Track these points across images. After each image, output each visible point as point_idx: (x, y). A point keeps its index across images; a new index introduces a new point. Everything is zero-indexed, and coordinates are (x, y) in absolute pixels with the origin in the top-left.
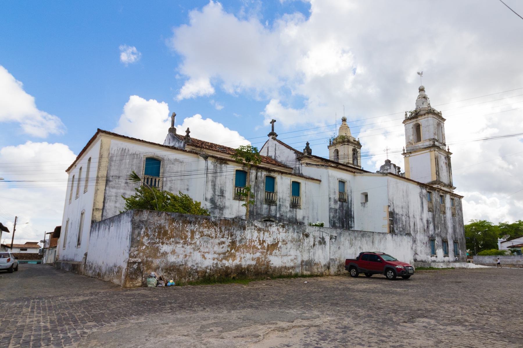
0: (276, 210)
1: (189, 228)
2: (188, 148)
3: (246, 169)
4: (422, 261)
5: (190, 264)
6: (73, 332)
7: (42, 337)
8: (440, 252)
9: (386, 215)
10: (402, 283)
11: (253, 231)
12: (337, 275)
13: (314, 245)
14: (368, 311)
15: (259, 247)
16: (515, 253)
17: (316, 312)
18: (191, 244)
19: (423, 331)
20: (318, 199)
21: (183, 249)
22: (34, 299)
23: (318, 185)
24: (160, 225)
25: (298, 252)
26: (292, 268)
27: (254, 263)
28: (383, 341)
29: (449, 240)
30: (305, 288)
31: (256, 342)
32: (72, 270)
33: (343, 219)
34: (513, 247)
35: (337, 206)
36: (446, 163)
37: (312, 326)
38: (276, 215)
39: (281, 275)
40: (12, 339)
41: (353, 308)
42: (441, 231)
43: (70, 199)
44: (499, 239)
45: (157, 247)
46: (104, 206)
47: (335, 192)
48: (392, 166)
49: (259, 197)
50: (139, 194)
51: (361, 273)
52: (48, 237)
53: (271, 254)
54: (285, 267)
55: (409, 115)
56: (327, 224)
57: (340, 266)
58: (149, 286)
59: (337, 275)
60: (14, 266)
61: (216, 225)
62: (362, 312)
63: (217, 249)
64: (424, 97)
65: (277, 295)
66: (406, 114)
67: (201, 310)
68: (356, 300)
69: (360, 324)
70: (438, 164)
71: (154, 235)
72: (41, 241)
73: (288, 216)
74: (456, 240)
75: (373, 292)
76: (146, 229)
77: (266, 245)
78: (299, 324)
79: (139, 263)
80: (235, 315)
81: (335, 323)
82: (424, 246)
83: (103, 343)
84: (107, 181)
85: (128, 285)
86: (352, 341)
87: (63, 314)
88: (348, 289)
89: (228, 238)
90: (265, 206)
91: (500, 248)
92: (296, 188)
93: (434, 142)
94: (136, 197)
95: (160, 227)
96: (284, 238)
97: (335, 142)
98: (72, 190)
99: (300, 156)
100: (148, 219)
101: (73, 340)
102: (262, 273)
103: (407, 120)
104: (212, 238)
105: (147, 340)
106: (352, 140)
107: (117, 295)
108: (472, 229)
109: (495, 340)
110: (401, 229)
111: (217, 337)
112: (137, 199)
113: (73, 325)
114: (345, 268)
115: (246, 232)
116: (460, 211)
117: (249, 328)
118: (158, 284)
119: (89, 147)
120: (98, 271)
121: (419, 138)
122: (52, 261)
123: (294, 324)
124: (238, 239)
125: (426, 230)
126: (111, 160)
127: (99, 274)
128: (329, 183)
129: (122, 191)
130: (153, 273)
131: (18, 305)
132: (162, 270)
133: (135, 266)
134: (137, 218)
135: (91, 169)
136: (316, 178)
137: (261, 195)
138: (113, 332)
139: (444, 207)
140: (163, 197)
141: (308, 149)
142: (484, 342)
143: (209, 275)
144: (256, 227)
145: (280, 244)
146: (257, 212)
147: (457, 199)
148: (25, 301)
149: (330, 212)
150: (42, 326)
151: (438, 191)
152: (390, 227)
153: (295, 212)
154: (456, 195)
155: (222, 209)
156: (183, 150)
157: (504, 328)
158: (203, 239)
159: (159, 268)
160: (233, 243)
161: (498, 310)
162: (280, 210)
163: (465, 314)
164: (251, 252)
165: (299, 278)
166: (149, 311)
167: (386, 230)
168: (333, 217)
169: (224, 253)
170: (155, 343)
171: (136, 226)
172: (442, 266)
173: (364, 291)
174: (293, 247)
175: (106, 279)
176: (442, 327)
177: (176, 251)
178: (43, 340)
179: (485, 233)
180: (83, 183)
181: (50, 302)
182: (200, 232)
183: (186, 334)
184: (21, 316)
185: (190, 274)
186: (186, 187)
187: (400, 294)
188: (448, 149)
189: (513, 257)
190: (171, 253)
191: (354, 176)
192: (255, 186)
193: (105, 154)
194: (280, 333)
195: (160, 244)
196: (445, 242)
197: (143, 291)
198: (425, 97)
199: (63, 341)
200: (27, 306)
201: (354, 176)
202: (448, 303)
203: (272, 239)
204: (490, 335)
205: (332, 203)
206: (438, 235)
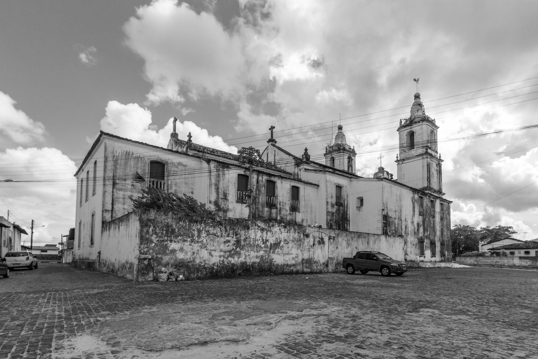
0: (277, 213)
1: (195, 227)
2: (191, 153)
3: (248, 173)
4: (411, 261)
5: (197, 261)
6: (87, 320)
7: (56, 324)
8: (428, 253)
9: (380, 218)
10: (398, 279)
11: (257, 230)
12: (335, 272)
13: (314, 245)
14: (372, 302)
15: (263, 246)
16: (495, 255)
17: (322, 303)
18: (198, 242)
19: (430, 320)
20: (315, 205)
21: (191, 247)
22: (50, 291)
23: (316, 189)
24: (168, 223)
25: (299, 251)
26: (294, 265)
27: (258, 260)
28: (394, 329)
30: (307, 283)
31: (269, 330)
32: (88, 267)
33: (339, 221)
34: (493, 249)
35: (334, 210)
36: (437, 170)
37: (321, 315)
38: (277, 217)
39: (283, 271)
40: (26, 326)
41: (357, 300)
43: (81, 202)
44: (480, 242)
45: (166, 245)
46: (113, 208)
47: (332, 196)
48: (385, 173)
49: (261, 201)
50: (146, 195)
51: (357, 270)
52: (65, 240)
53: (274, 252)
54: (287, 265)
56: (324, 226)
57: (337, 264)
58: (161, 280)
59: (335, 272)
60: (34, 264)
61: (221, 224)
62: (367, 303)
63: (222, 247)
65: (282, 288)
66: (401, 122)
67: (212, 301)
68: (358, 293)
69: (368, 314)
71: (162, 234)
72: (59, 244)
73: (288, 219)
75: (373, 286)
76: (154, 227)
77: (268, 244)
78: (308, 313)
79: (150, 259)
80: (244, 305)
81: (343, 312)
82: (414, 247)
83: (116, 329)
84: (114, 184)
85: (140, 280)
86: (363, 329)
87: (78, 304)
88: (349, 284)
89: (233, 237)
90: (266, 209)
91: (480, 251)
92: (295, 192)
93: (427, 150)
94: (142, 198)
95: (168, 226)
96: (286, 238)
97: (331, 149)
98: (81, 193)
99: (298, 162)
100: (156, 218)
101: (86, 327)
102: (265, 270)
103: (402, 127)
104: (218, 236)
105: (160, 327)
106: (347, 148)
107: (130, 288)
108: (455, 233)
109: (504, 328)
110: (394, 232)
111: (229, 324)
112: (144, 200)
113: (87, 314)
114: (342, 266)
115: (250, 232)
117: (260, 317)
118: (168, 279)
119: (94, 151)
120: (111, 268)
121: (412, 145)
122: (71, 261)
123: (303, 313)
124: (242, 238)
125: (416, 233)
126: (116, 162)
127: (113, 271)
128: (327, 187)
129: (129, 193)
130: (163, 269)
131: (35, 296)
132: (172, 266)
133: (146, 262)
134: (145, 217)
135: (98, 169)
136: (314, 183)
137: (263, 199)
138: (126, 320)
139: (434, 211)
140: (168, 198)
141: (306, 155)
142: (494, 329)
143: (217, 272)
144: (259, 227)
145: (282, 243)
146: (259, 215)
147: (446, 205)
148: (42, 293)
149: (327, 216)
150: (57, 314)
152: (383, 230)
153: (294, 215)
154: (445, 200)
155: (226, 211)
156: (186, 154)
157: (508, 317)
158: (209, 237)
159: (168, 264)
160: (238, 242)
161: (496, 301)
162: (280, 213)
163: (465, 305)
164: (255, 250)
165: (300, 275)
166: (161, 301)
167: (380, 232)
168: (330, 220)
169: (230, 251)
170: (168, 330)
171: (144, 224)
172: (429, 265)
173: (364, 285)
174: (294, 246)
175: (120, 274)
176: (448, 317)
177: (184, 248)
178: (57, 327)
179: (467, 238)
180: (91, 183)
181: (66, 294)
182: (206, 231)
183: (198, 322)
184: (37, 306)
185: (198, 270)
186: (191, 190)
187: (399, 288)
188: (440, 157)
189: (492, 258)
190: (180, 250)
191: (351, 181)
192: (256, 190)
193: (110, 155)
194: (291, 321)
195: (169, 242)
197: (155, 285)
198: (420, 105)
199: (76, 328)
200: (44, 298)
201: (351, 181)
202: (446, 296)
203: (274, 238)
204: (496, 323)
205: (329, 207)
206: (427, 237)
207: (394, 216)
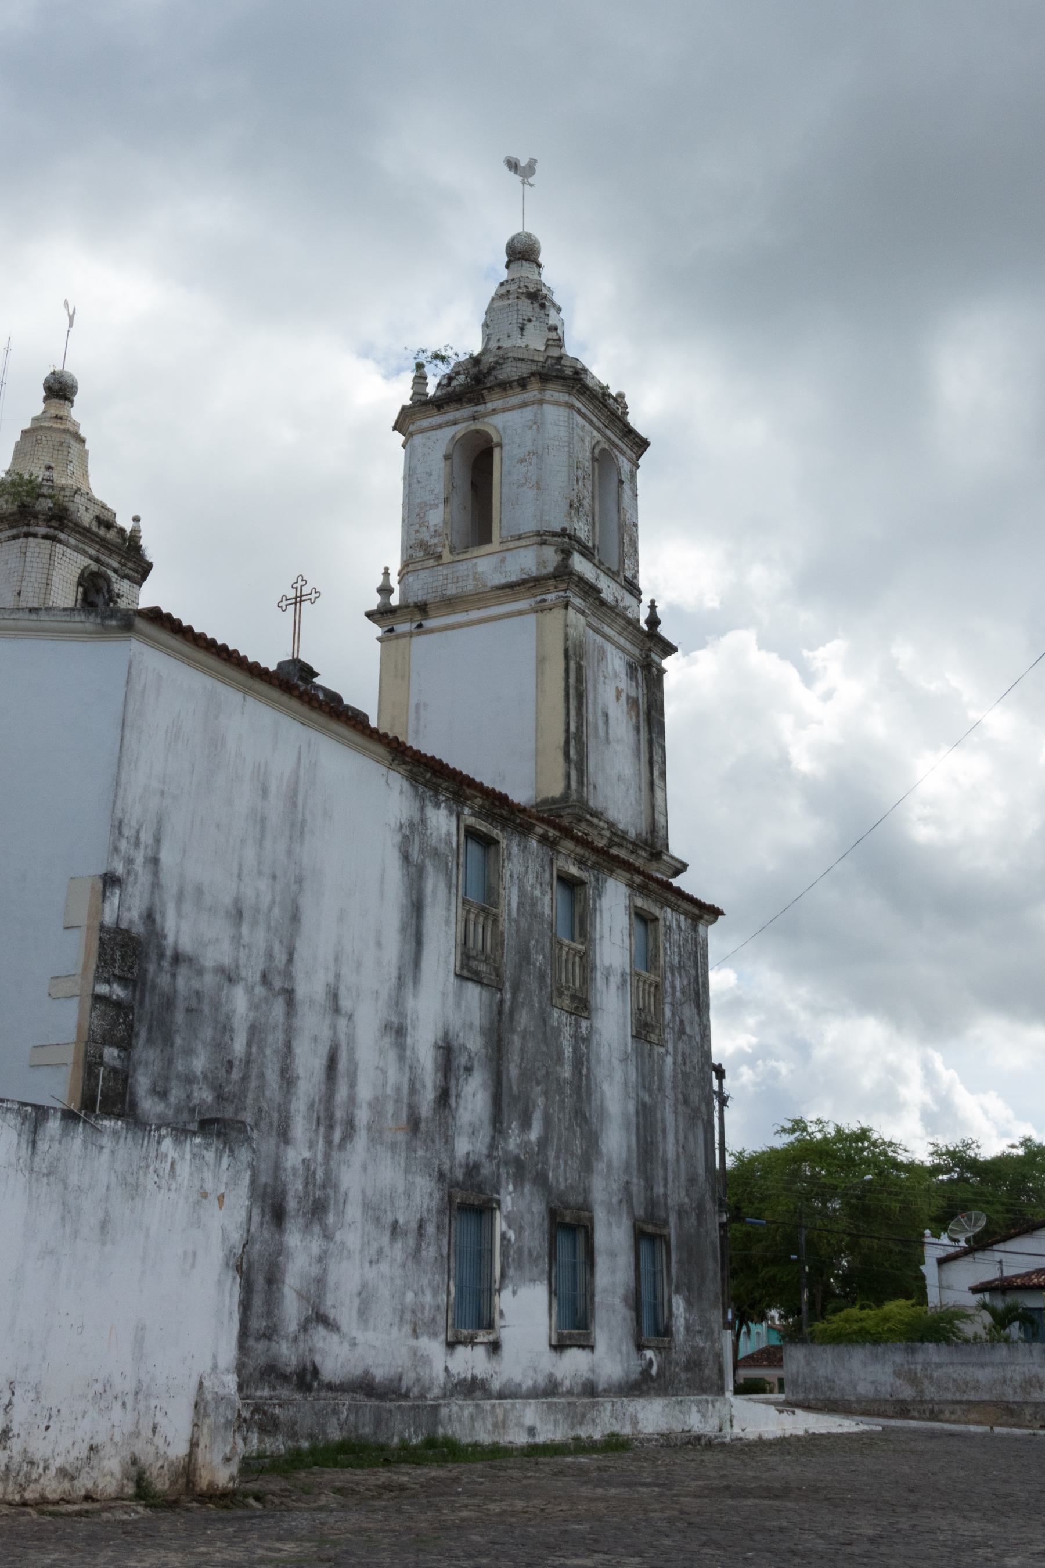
4: (365, 1387)
8: (525, 1310)
9: (73, 953)
16: (1015, 1330)
29: (600, 1216)
36: (633, 702)
42: (544, 1142)
70: (580, 696)
74: (651, 1217)
82: (398, 1251)
91: (933, 1296)
93: (567, 553)
106: (86, 518)
108: (796, 1174)
110: (204, 1095)
116: (688, 1011)
125: (424, 1124)
139: (586, 962)
151: (543, 839)
152: (91, 1066)
172: (531, 1424)
188: (654, 621)
189: (1002, 1352)
196: (572, 1229)
198: (538, 298)
206: (519, 1169)
207: (214, 956)
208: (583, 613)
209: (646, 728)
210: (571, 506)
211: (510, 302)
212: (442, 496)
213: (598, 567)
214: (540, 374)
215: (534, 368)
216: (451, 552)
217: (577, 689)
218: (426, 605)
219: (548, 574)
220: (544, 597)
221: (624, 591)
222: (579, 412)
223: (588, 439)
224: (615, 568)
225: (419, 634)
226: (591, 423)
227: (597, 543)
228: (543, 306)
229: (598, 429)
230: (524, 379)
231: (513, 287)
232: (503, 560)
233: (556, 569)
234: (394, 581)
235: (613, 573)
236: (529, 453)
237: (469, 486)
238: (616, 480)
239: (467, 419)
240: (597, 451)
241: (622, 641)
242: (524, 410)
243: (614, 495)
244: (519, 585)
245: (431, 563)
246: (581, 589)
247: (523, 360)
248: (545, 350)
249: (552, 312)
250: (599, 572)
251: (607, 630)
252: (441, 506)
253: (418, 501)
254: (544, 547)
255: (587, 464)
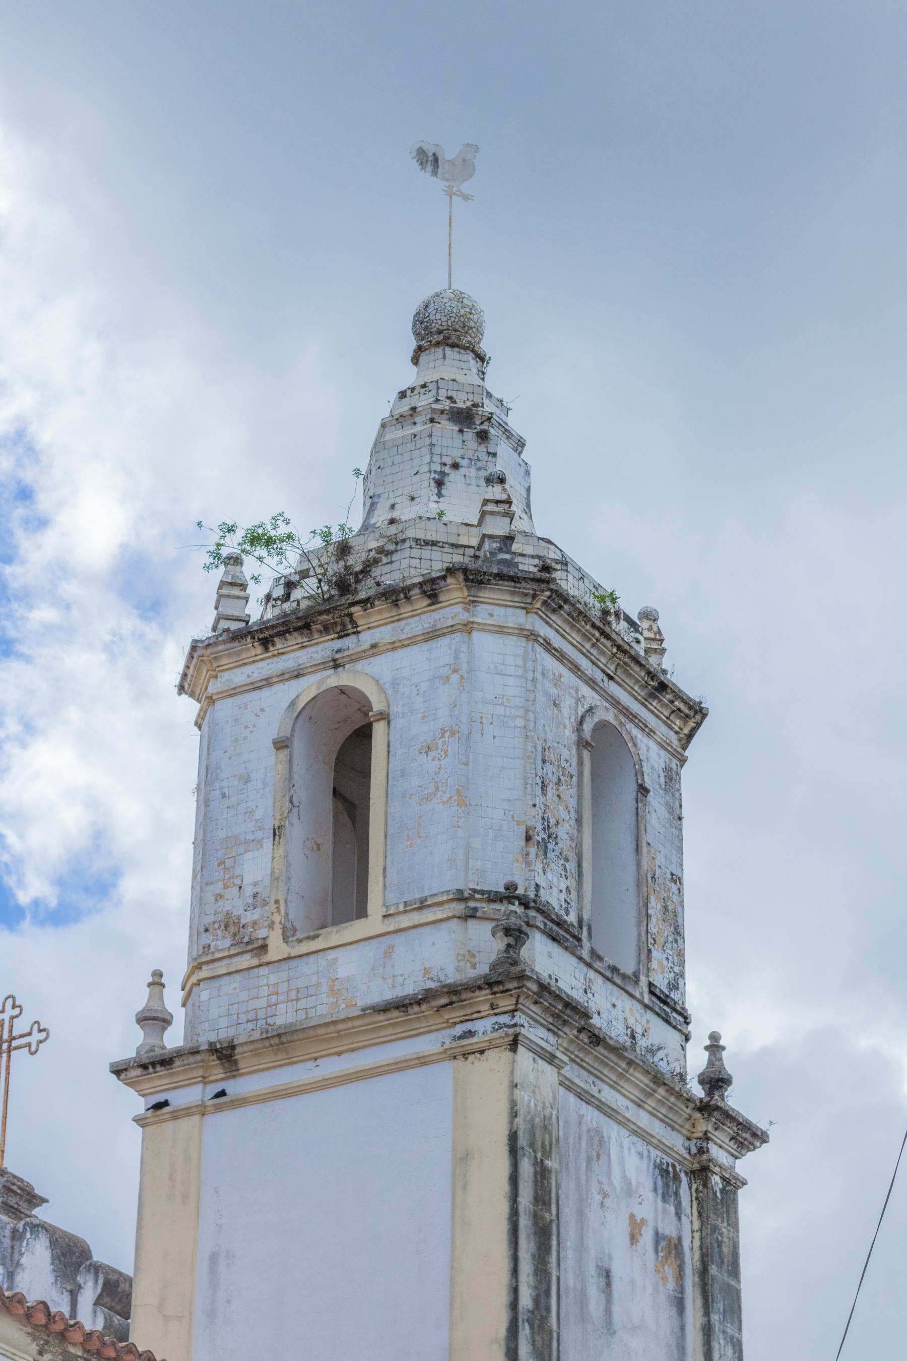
36: (670, 1248)
55: (263, 573)
64: (463, 417)
70: (544, 1234)
93: (515, 935)
121: (345, 888)
188: (716, 1081)
208: (551, 1059)
209: (699, 1302)
210: (528, 839)
211: (416, 429)
212: (269, 824)
213: (589, 965)
214: (465, 571)
215: (457, 559)
216: (285, 939)
217: (536, 1217)
218: (233, 1047)
219: (476, 979)
220: (469, 1026)
221: (649, 1015)
222: (547, 646)
223: (567, 703)
224: (628, 968)
225: (219, 1108)
226: (576, 669)
227: (586, 917)
228: (483, 436)
229: (591, 683)
230: (433, 581)
231: (423, 401)
232: (389, 953)
233: (493, 967)
234: (173, 999)
235: (624, 977)
236: (443, 731)
237: (328, 802)
238: (633, 787)
239: (321, 666)
240: (588, 727)
241: (643, 1120)
242: (433, 644)
243: (629, 818)
244: (419, 1003)
245: (246, 961)
246: (546, 1010)
247: (434, 543)
248: (480, 524)
249: (503, 448)
250: (592, 974)
251: (608, 1095)
252: (268, 844)
253: (222, 834)
254: (471, 923)
255: (565, 754)
